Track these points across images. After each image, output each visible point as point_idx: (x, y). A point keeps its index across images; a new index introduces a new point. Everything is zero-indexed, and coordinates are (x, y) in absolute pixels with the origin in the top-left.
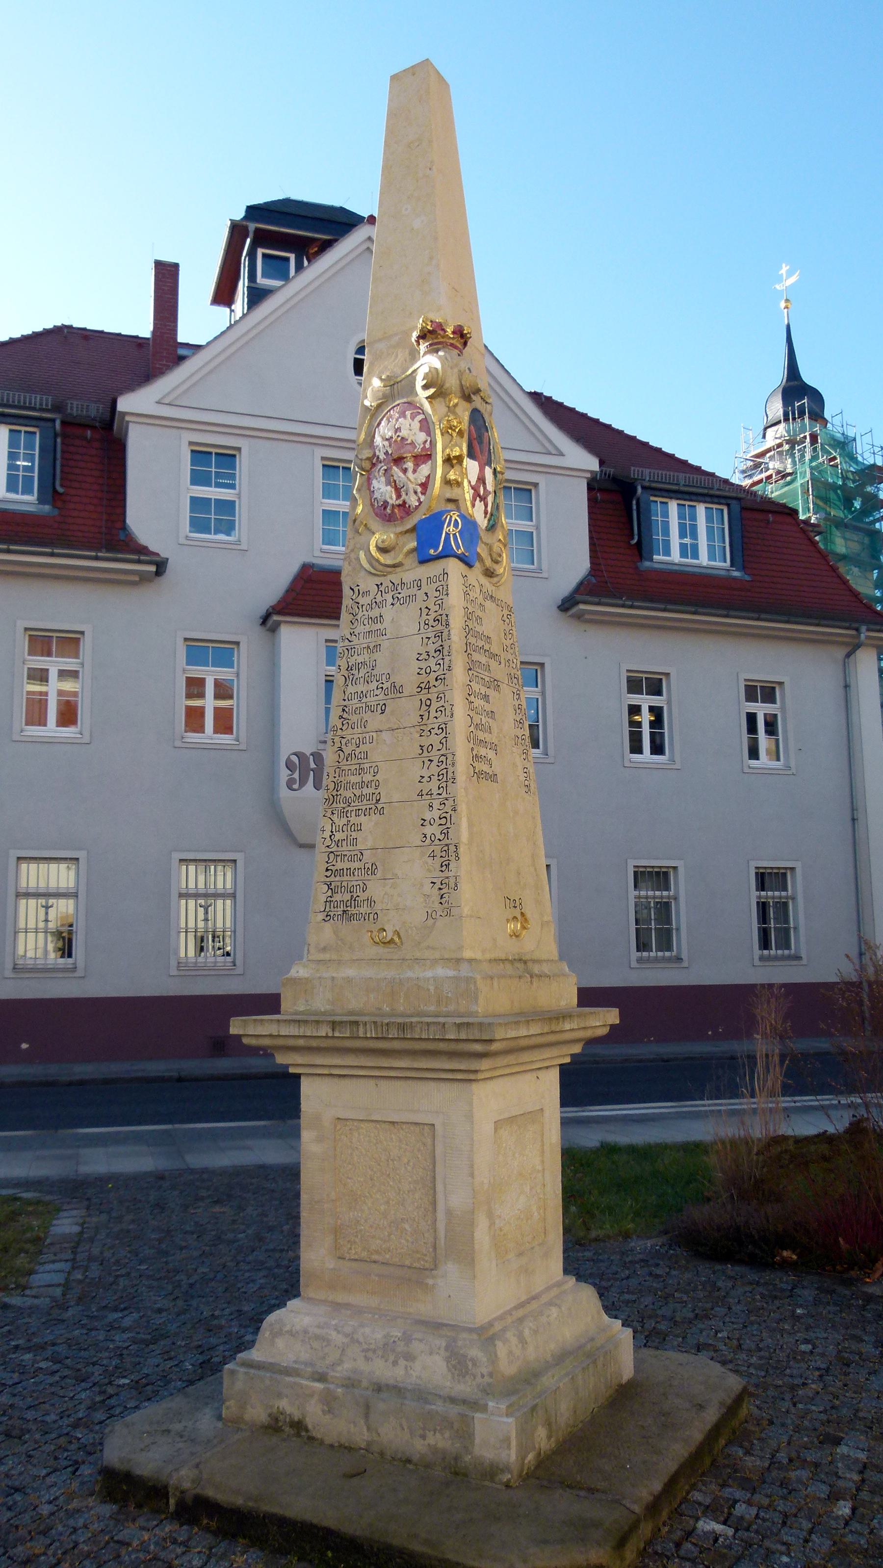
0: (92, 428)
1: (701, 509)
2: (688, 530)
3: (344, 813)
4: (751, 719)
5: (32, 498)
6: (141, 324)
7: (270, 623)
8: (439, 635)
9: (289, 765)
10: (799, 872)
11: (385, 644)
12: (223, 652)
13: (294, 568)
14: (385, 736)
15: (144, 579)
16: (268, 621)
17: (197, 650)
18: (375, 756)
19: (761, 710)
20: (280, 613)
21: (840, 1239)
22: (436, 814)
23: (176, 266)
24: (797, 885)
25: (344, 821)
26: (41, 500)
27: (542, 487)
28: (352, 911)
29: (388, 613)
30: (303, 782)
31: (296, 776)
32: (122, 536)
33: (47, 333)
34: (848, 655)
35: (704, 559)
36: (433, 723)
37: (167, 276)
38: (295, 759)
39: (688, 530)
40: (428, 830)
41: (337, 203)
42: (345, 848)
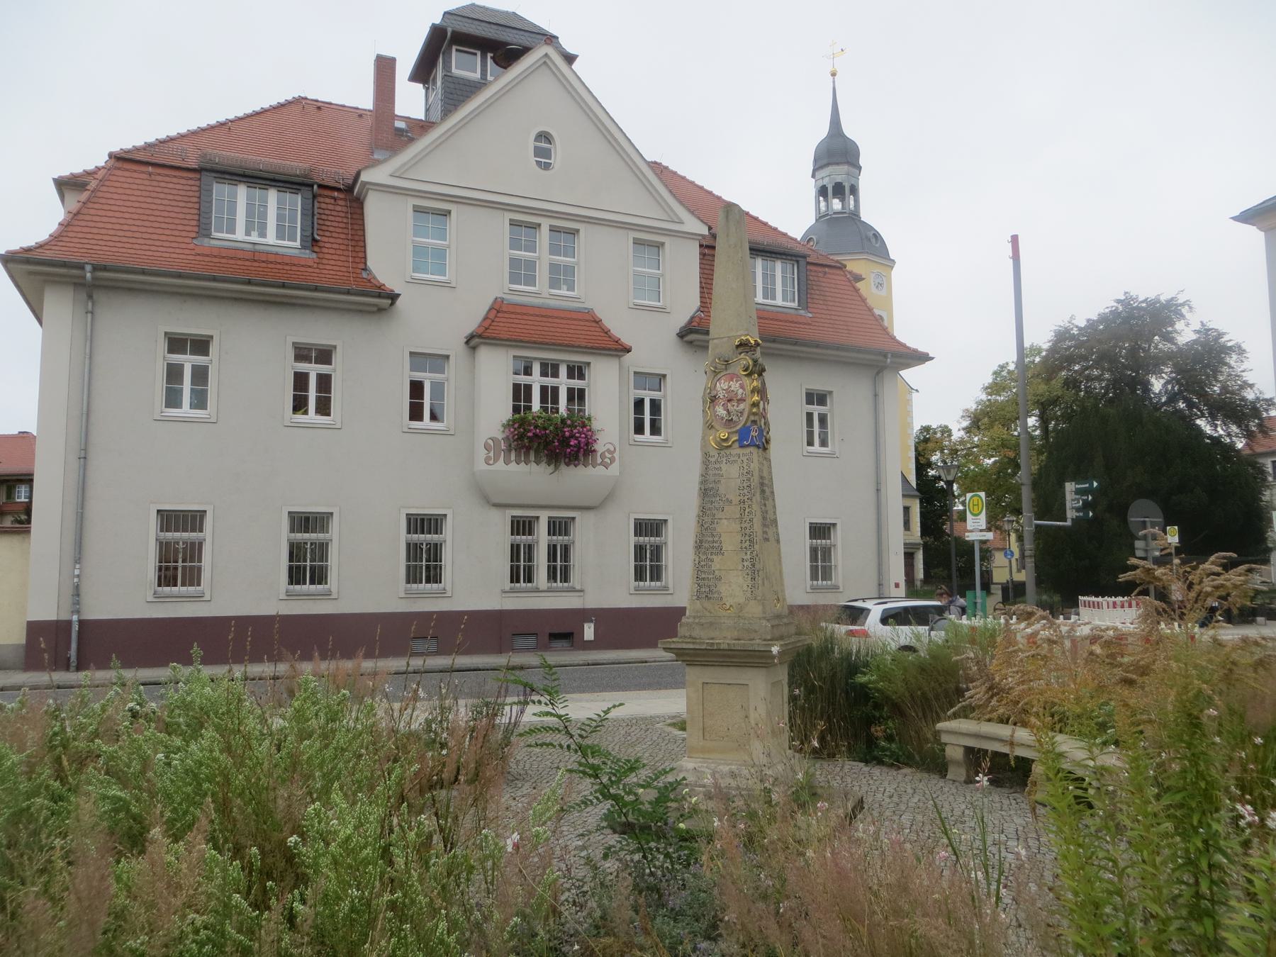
0: (338, 190)
1: (779, 265)
2: (769, 278)
3: (705, 553)
4: (810, 416)
5: (298, 244)
6: (366, 101)
7: (473, 342)
8: (749, 480)
9: (487, 447)
10: (838, 527)
12: (439, 361)
13: (490, 301)
14: (725, 522)
15: (381, 310)
16: (474, 341)
17: (418, 359)
18: (718, 530)
19: (816, 410)
20: (480, 336)
21: (1201, 422)
23: (393, 60)
24: (838, 537)
26: (303, 247)
27: (667, 246)
29: (724, 466)
30: (496, 460)
31: (492, 454)
32: (364, 275)
33: (289, 103)
34: (878, 373)
35: (779, 301)
36: (746, 518)
37: (385, 67)
38: (491, 442)
39: (769, 278)
41: (510, 10)
42: (705, 569)
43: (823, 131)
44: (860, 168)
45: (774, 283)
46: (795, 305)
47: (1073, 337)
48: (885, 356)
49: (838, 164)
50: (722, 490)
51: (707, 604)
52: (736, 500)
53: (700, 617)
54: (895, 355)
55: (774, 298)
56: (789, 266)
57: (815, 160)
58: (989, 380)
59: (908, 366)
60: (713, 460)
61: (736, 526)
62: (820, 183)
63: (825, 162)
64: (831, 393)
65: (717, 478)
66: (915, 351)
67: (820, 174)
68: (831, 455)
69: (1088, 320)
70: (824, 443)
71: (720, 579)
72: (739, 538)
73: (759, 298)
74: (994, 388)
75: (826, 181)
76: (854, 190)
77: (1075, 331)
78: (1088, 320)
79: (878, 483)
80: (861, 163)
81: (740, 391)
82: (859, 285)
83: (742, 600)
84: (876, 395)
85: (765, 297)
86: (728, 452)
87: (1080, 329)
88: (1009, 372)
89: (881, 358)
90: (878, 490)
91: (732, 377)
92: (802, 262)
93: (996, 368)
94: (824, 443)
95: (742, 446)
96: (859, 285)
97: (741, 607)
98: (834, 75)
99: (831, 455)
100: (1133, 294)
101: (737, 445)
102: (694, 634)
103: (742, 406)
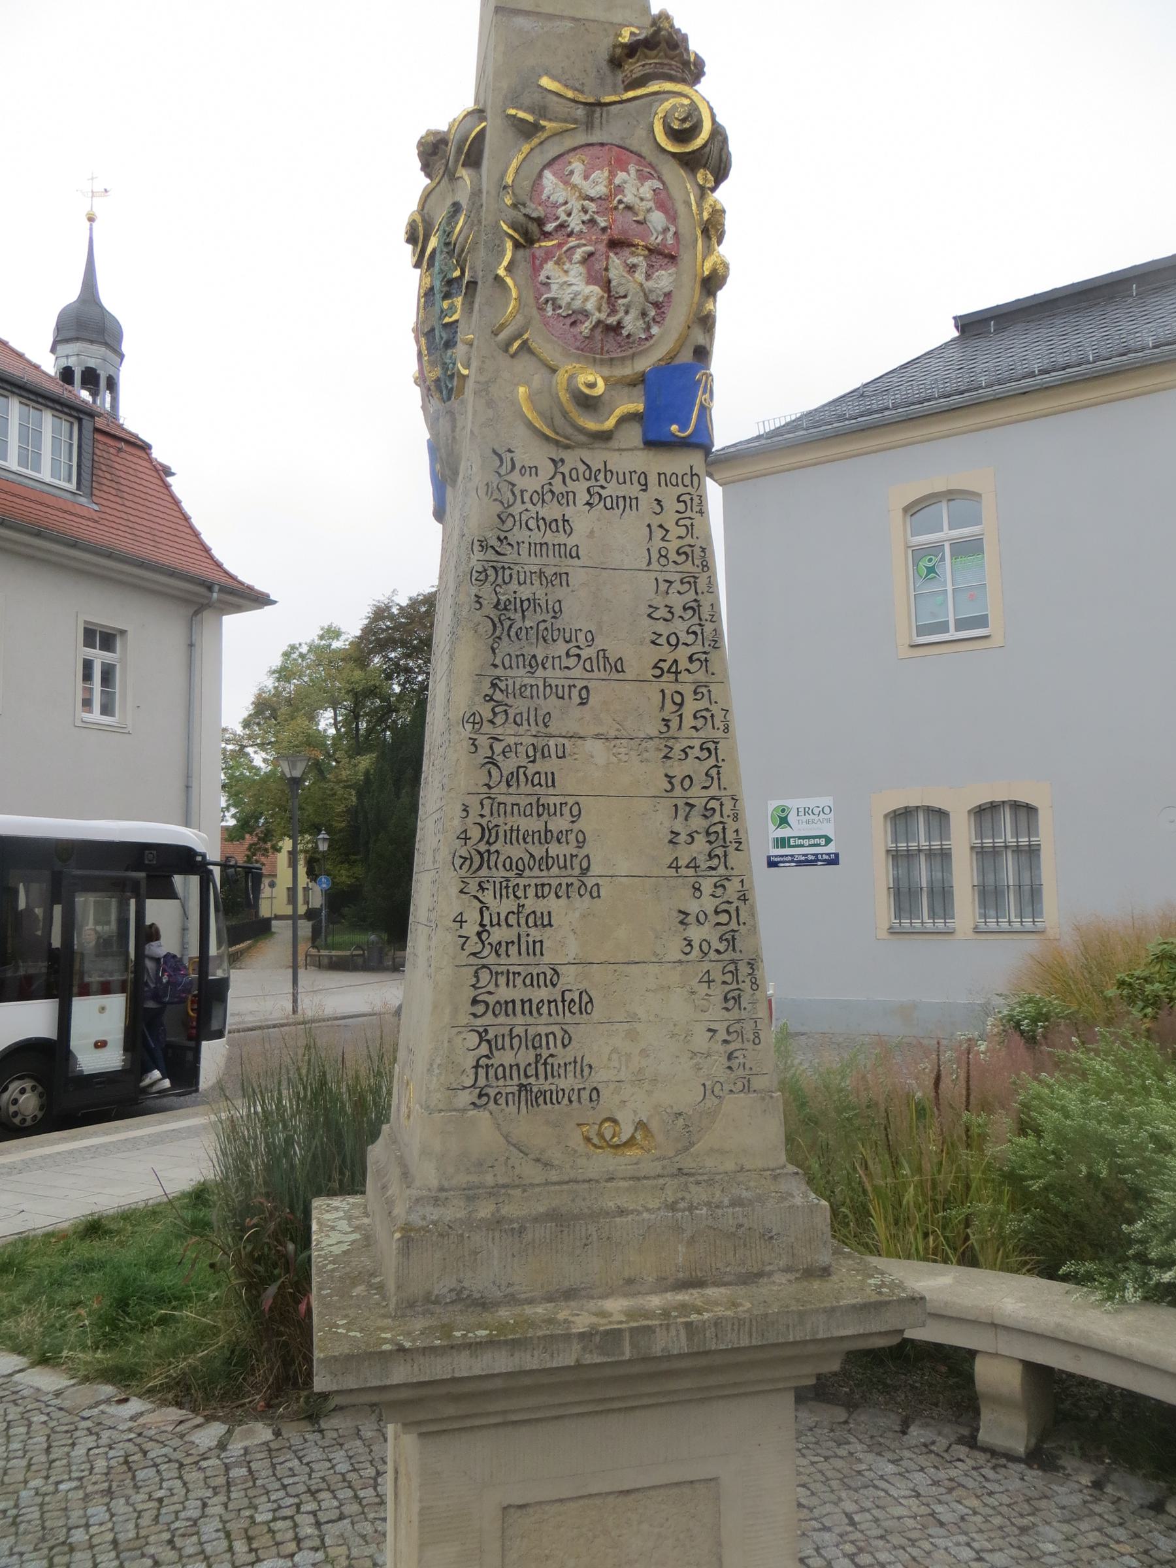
2: (30, 437)
3: (505, 889)
4: (88, 665)
11: (578, 576)
14: (595, 748)
18: (568, 783)
19: (99, 657)
22: (709, 904)
25: (509, 904)
28: (537, 1084)
29: (583, 520)
34: (196, 613)
36: (687, 737)
39: (30, 437)
40: (696, 933)
42: (514, 960)
43: (71, 293)
44: (122, 356)
45: (38, 444)
46: (72, 487)
47: (392, 617)
48: (210, 588)
49: (92, 342)
50: (576, 616)
51: (529, 1126)
52: (639, 659)
53: (495, 1192)
54: (224, 589)
55: (37, 468)
56: (65, 426)
57: (59, 328)
58: (277, 662)
59: (239, 609)
60: (530, 484)
61: (647, 773)
62: (64, 363)
63: (72, 334)
64: (123, 632)
65: (552, 564)
66: (250, 588)
67: (64, 349)
68: (119, 730)
69: (410, 599)
70: (106, 710)
71: (584, 1004)
72: (662, 821)
73: (12, 463)
74: (283, 674)
75: (71, 362)
76: (112, 385)
77: (395, 611)
78: (410, 599)
79: (188, 776)
80: (125, 348)
81: (657, 219)
82: (169, 479)
83: (686, 1096)
84: (191, 645)
85: (23, 462)
86: (596, 458)
87: (401, 608)
88: (302, 656)
89: (202, 590)
90: (188, 787)
91: (621, 156)
92: (87, 423)
93: (286, 648)
94: (107, 709)
95: (651, 444)
96: (169, 479)
97: (688, 1127)
98: (91, 219)
99: (119, 730)
100: (414, 595)
101: (633, 435)
102: (480, 1282)
103: (664, 279)
